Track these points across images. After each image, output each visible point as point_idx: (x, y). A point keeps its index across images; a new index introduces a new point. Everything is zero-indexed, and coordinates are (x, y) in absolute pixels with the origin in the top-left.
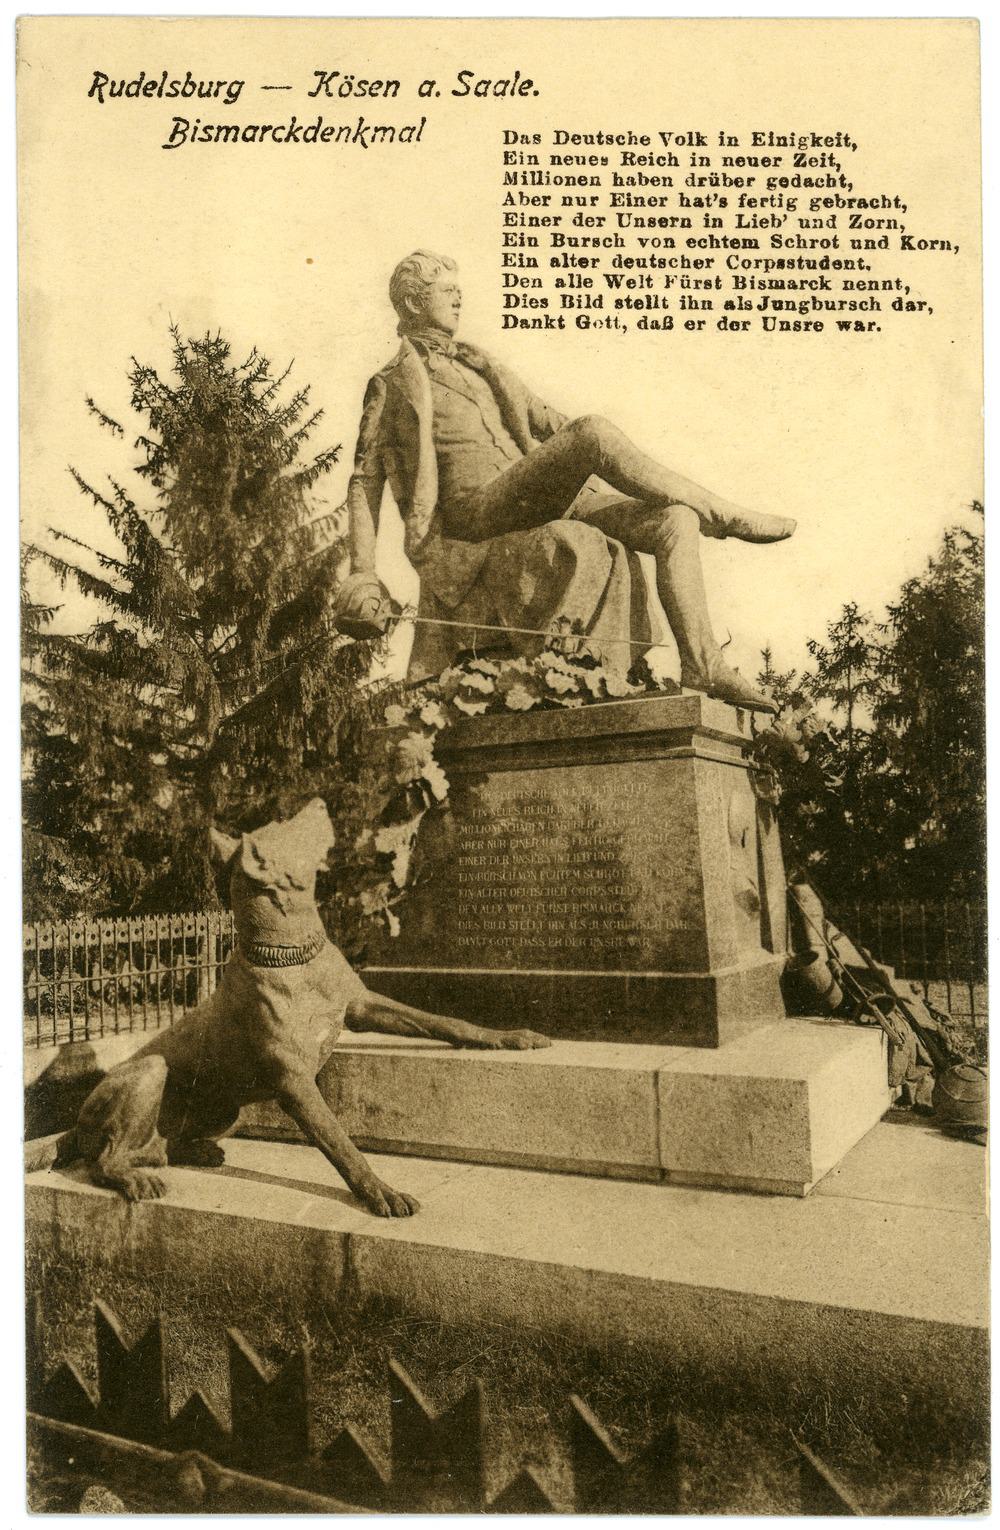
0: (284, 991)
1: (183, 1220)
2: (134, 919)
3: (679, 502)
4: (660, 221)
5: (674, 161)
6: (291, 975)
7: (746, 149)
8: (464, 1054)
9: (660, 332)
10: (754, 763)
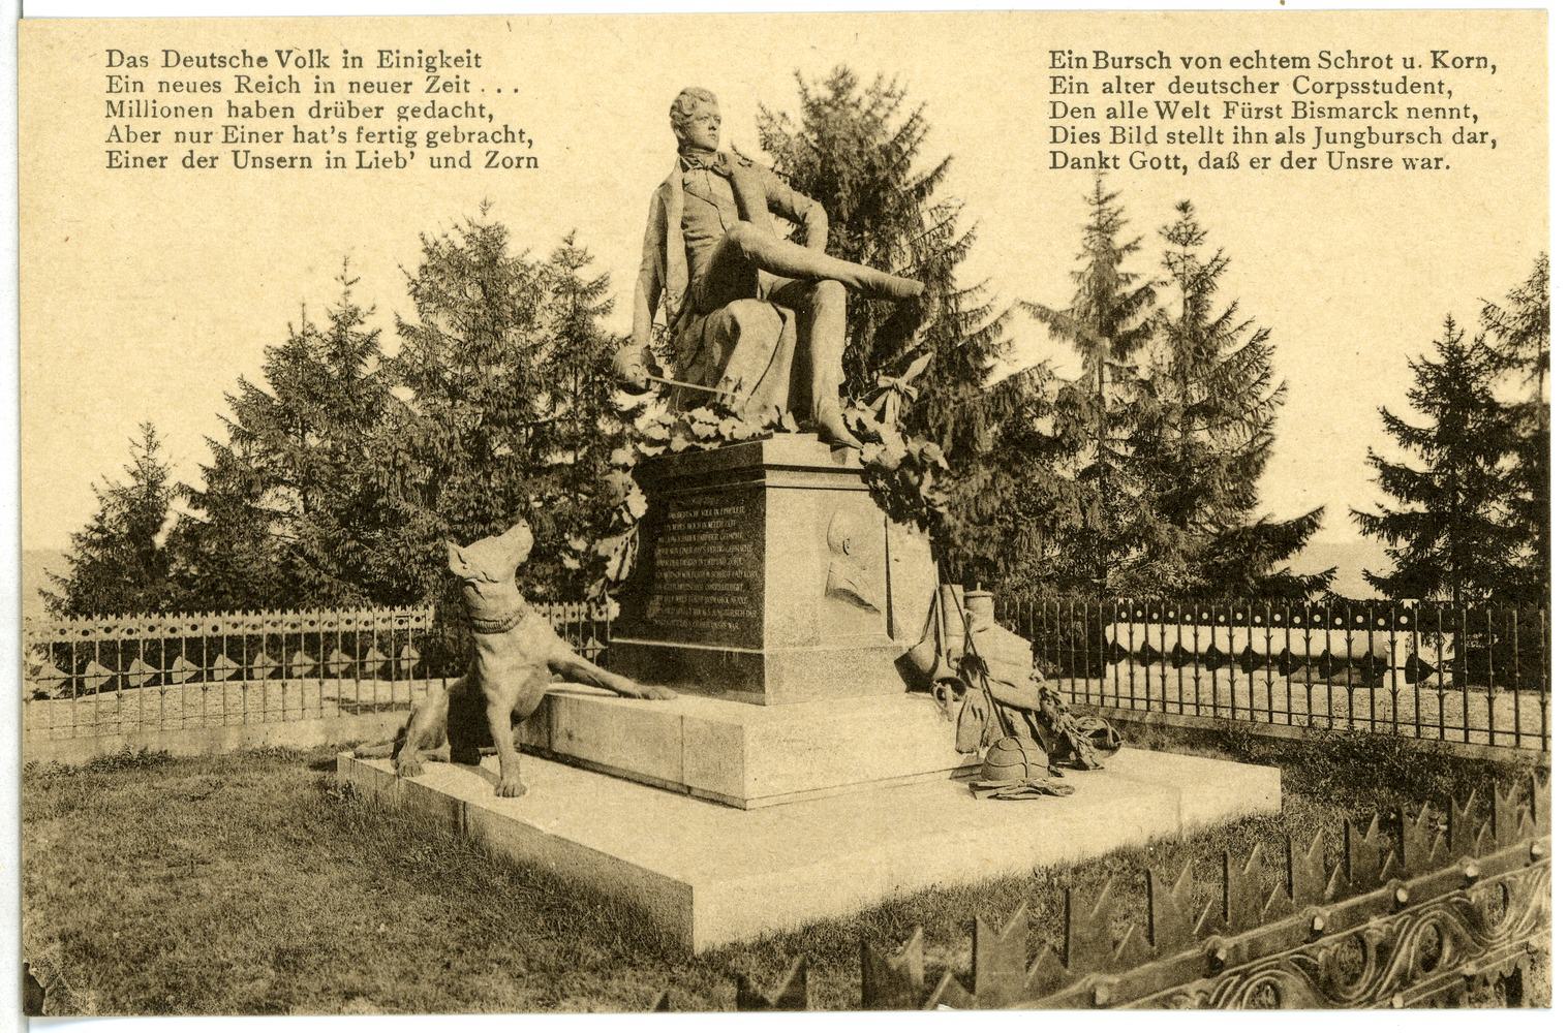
4: (280, 160)
5: (294, 86)
7: (370, 72)
9: (1225, 172)
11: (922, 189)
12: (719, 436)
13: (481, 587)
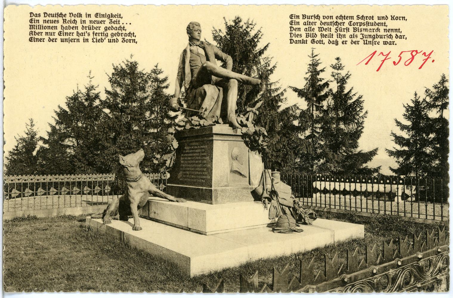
0: (131, 186)
1: (112, 229)
2: (155, 174)
3: (233, 78)
6: (132, 184)
8: (171, 203)
10: (38, 148)
11: (261, 52)
12: (200, 125)
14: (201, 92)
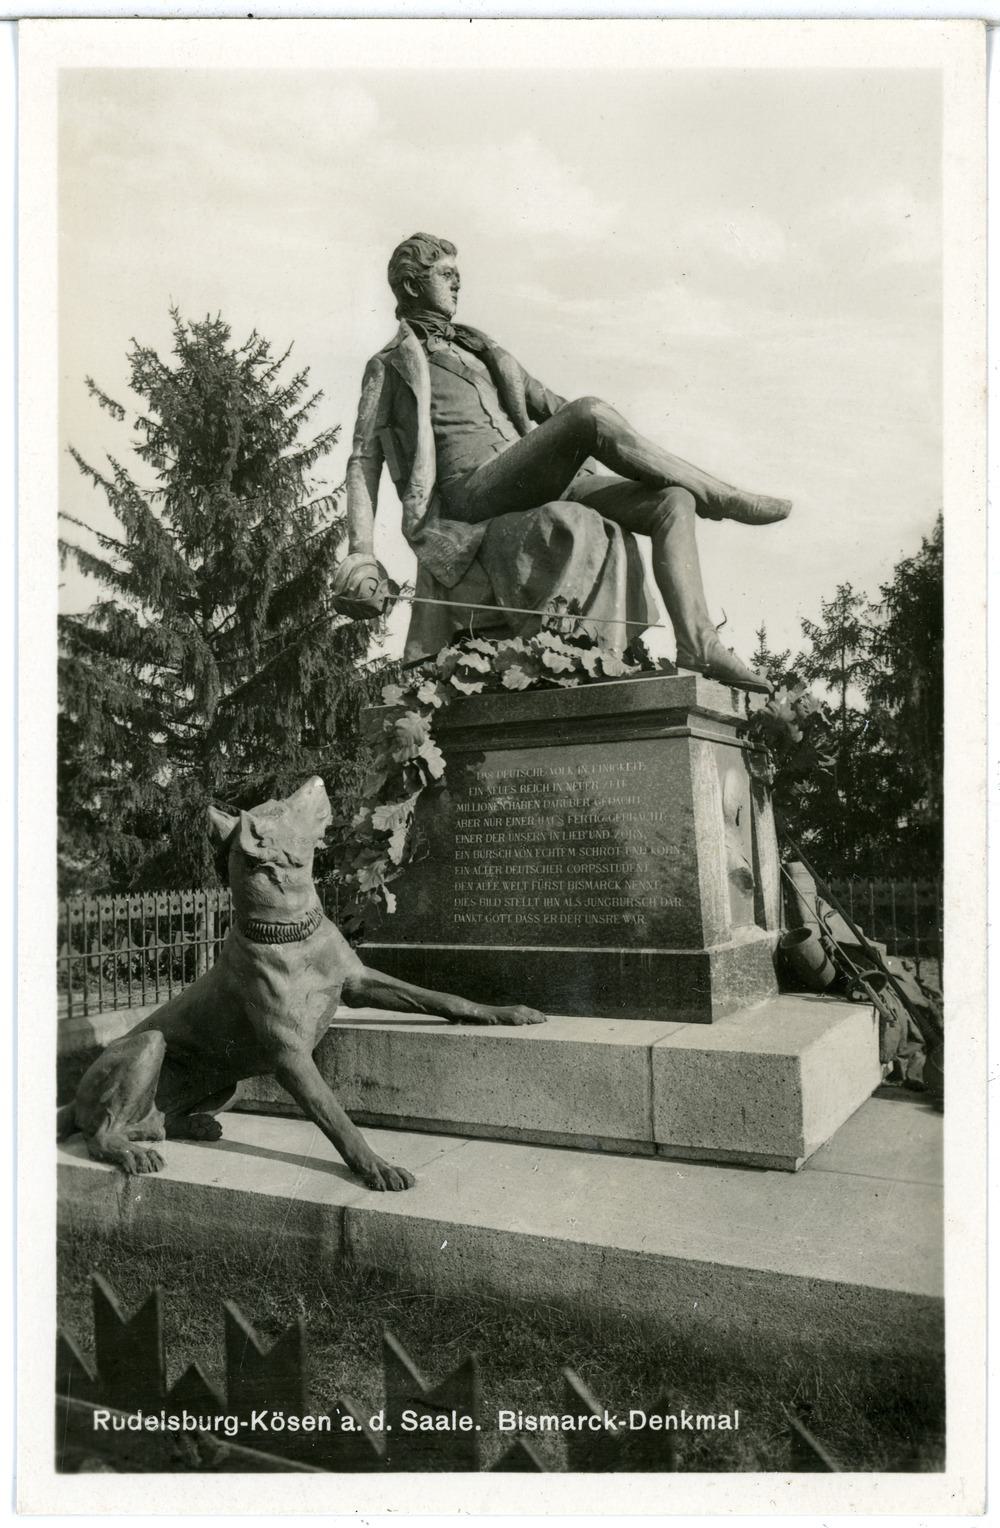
0: (281, 967)
8: (459, 1030)
11: (303, 460)
12: (580, 672)
13: (280, 873)
14: (537, 533)
